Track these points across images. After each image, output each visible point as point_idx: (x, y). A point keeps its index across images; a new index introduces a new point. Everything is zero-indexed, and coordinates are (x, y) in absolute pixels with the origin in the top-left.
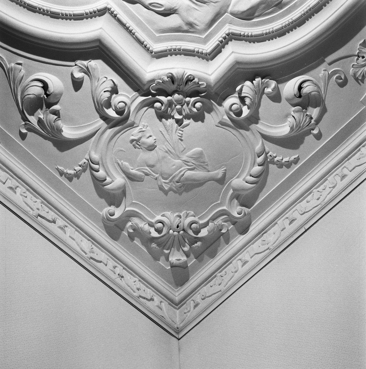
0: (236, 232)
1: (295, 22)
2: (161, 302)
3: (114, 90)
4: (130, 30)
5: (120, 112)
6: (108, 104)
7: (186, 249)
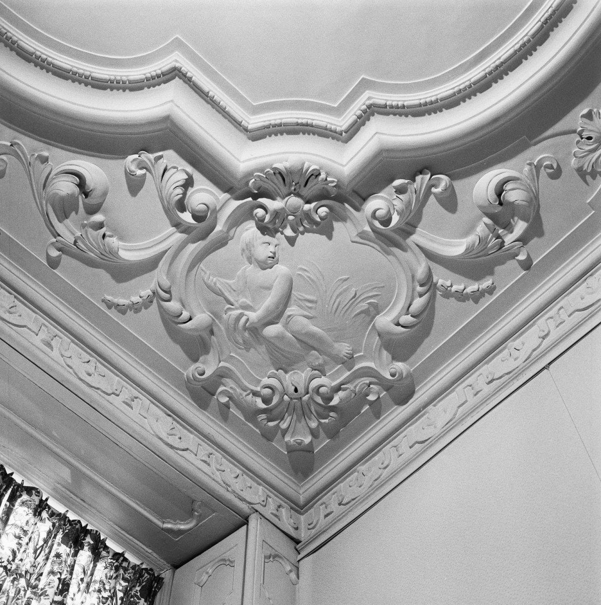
0: (390, 401)
1: (474, 85)
2: (279, 507)
3: (188, 183)
4: (210, 97)
5: (198, 218)
6: (181, 206)
7: (314, 425)
